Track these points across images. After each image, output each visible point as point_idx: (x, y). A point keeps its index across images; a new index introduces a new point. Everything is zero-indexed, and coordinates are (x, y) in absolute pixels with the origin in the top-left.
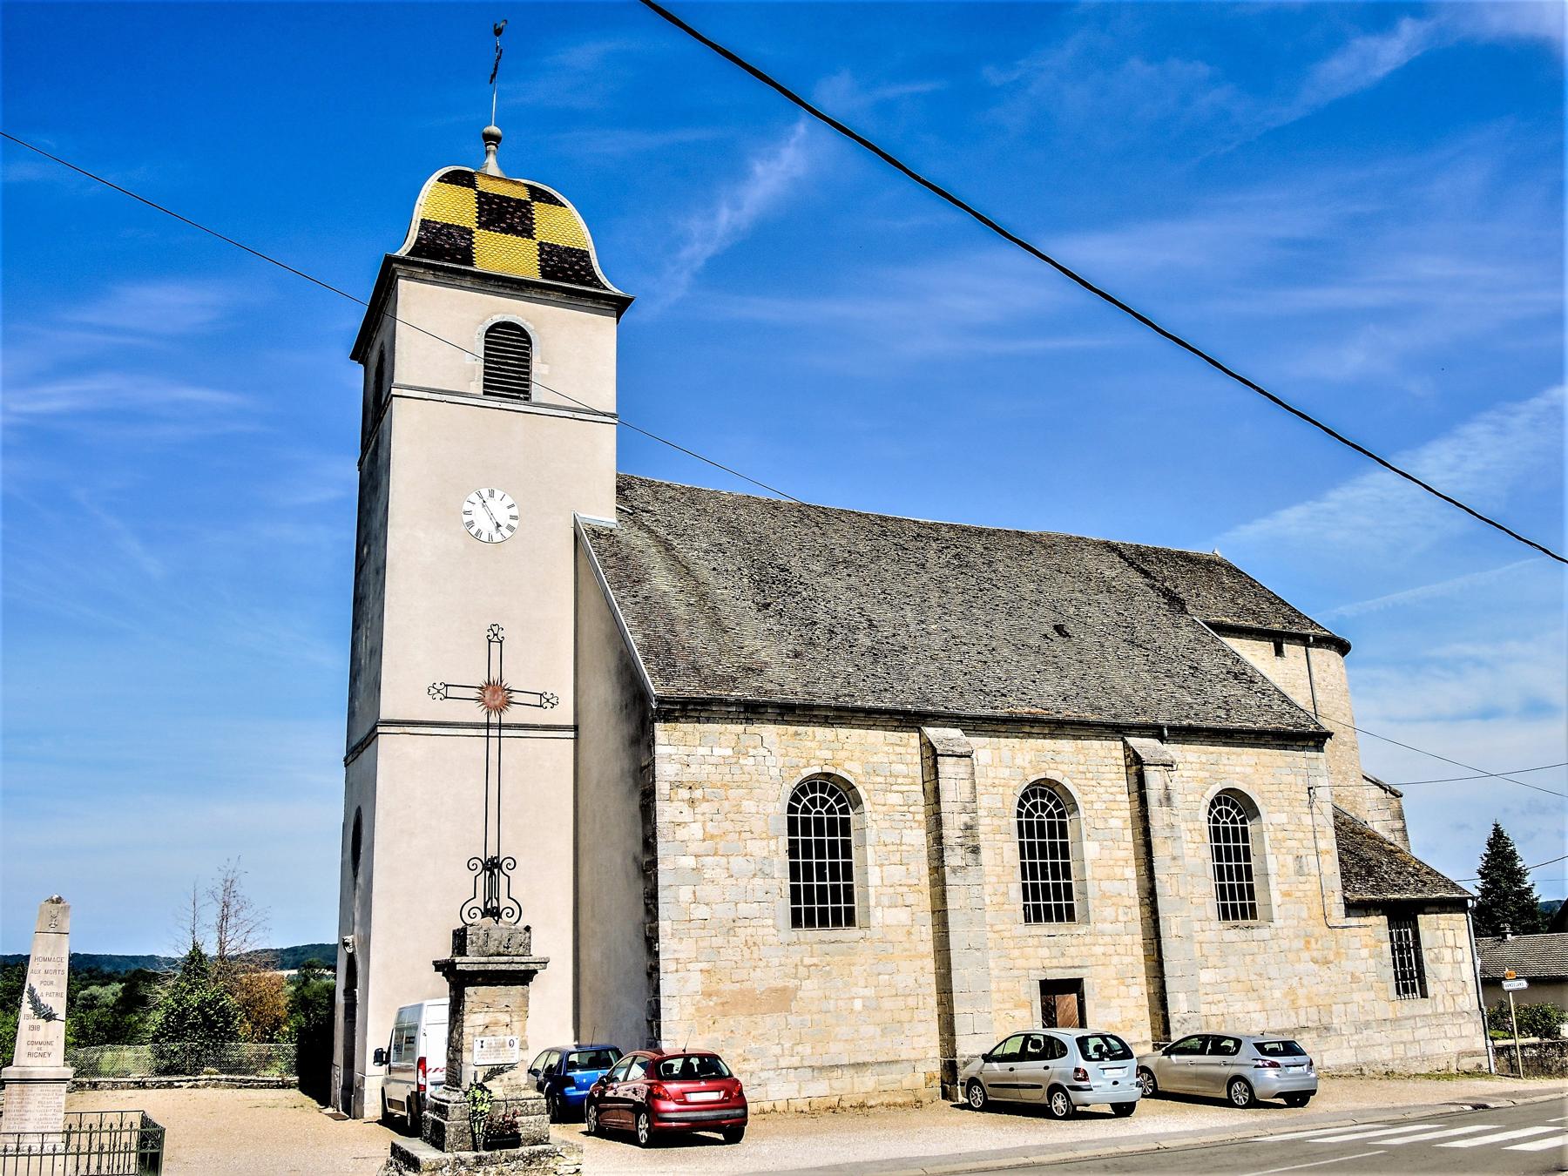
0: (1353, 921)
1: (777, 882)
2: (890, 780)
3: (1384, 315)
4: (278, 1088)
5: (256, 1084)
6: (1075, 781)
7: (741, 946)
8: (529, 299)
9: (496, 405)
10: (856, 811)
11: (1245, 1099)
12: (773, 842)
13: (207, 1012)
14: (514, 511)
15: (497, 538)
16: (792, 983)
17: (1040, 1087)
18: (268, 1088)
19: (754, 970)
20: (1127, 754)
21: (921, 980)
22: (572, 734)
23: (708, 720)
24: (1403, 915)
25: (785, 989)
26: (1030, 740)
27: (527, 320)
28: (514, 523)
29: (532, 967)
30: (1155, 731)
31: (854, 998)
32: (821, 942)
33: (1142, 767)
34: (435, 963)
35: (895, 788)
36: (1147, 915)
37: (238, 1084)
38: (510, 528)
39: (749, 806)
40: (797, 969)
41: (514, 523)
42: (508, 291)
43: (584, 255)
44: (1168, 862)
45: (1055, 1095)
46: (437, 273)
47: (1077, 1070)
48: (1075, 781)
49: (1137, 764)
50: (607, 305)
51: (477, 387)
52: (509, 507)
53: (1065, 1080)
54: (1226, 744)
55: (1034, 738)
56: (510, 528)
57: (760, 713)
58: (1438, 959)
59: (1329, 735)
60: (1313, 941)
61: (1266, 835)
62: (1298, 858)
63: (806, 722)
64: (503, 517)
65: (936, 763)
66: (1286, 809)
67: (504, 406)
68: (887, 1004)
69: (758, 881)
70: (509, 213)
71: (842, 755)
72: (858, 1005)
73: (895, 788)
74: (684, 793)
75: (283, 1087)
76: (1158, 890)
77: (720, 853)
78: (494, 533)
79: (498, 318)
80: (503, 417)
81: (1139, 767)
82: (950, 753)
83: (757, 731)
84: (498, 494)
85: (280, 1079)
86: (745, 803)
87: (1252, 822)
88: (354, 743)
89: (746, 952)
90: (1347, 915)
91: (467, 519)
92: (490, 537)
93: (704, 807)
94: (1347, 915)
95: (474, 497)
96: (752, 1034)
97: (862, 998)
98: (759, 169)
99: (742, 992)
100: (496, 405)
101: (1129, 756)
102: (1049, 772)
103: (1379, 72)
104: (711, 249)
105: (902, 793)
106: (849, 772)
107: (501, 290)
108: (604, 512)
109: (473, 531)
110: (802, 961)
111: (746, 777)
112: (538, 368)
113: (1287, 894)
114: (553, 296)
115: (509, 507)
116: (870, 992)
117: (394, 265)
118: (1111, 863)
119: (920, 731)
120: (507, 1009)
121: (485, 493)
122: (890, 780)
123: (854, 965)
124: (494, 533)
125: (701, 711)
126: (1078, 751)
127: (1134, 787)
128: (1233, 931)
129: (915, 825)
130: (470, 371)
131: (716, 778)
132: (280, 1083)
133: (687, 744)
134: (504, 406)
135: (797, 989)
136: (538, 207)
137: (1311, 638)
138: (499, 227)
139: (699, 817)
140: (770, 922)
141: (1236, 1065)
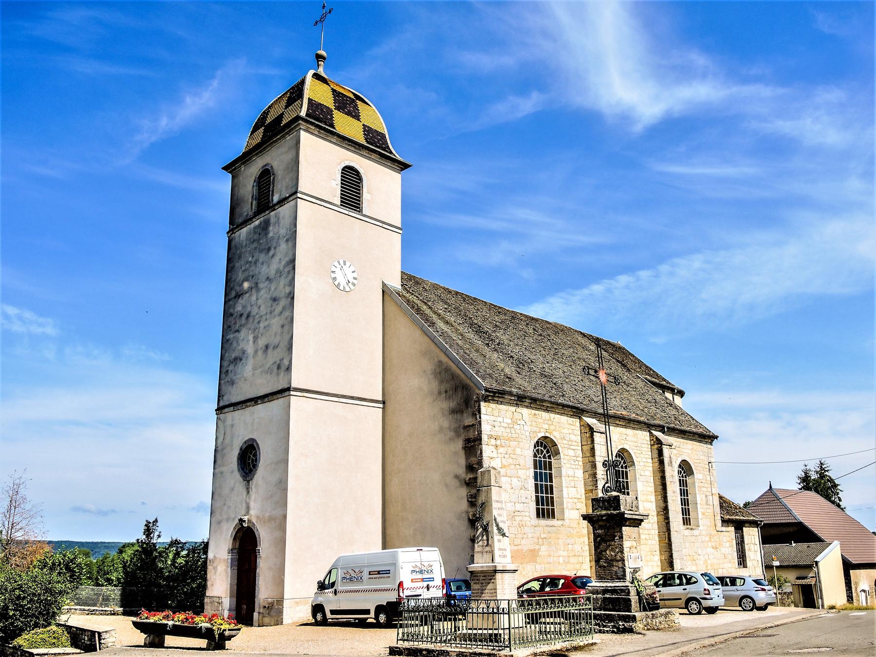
0: (724, 529)
1: (529, 493)
2: (570, 443)
3: (508, 236)
4: (111, 615)
5: (98, 612)
6: (634, 451)
7: (517, 526)
8: (362, 155)
9: (347, 212)
10: (555, 458)
11: (750, 607)
12: (528, 471)
13: (71, 565)
14: (355, 275)
15: (347, 289)
16: (537, 547)
17: (681, 599)
18: (105, 615)
19: (522, 539)
20: (651, 439)
21: (584, 548)
22: (381, 406)
23: (501, 403)
24: (739, 526)
25: (534, 550)
26: (618, 428)
27: (361, 167)
28: (355, 282)
29: (642, 518)
30: (662, 429)
31: (560, 556)
32: (547, 526)
33: (661, 446)
34: (582, 516)
35: (572, 447)
36: (662, 520)
37: (87, 612)
38: (354, 285)
39: (518, 451)
40: (538, 540)
41: (355, 282)
42: (352, 149)
43: (383, 136)
44: (672, 494)
45: (691, 603)
46: (321, 131)
47: (705, 590)
48: (634, 451)
49: (657, 444)
50: (397, 166)
51: (338, 201)
52: (353, 272)
53: (698, 594)
54: (682, 438)
55: (619, 427)
56: (354, 285)
57: (522, 401)
58: (749, 550)
59: (716, 437)
60: (712, 537)
61: (696, 484)
62: (706, 496)
63: (539, 408)
64: (350, 277)
65: (592, 436)
66: (702, 472)
67: (351, 214)
68: (572, 560)
69: (523, 492)
70: (348, 104)
71: (552, 427)
72: (561, 561)
73: (572, 447)
74: (493, 442)
75: (114, 614)
76: (670, 508)
77: (508, 475)
78: (346, 286)
79: (347, 163)
80: (346, 220)
81: (660, 445)
82: (598, 431)
83: (520, 411)
84: (348, 264)
85: (112, 609)
86: (517, 449)
87: (689, 477)
88: (221, 404)
89: (519, 529)
90: (722, 526)
91: (333, 275)
92: (344, 288)
93: (501, 450)
94: (722, 526)
95: (336, 264)
96: (523, 574)
97: (563, 556)
98: (188, 100)
99: (518, 551)
100: (347, 212)
101: (653, 440)
102: (625, 445)
103: (520, 115)
104: (154, 139)
105: (574, 450)
106: (555, 437)
107: (350, 148)
108: (395, 283)
109: (336, 283)
110: (540, 536)
111: (517, 436)
112: (366, 196)
113: (703, 514)
114: (374, 156)
115: (353, 272)
116: (565, 553)
117: (300, 122)
118: (646, 493)
119: (580, 418)
120: (635, 539)
121: (342, 263)
122: (570, 443)
123: (558, 539)
124: (346, 286)
125: (500, 397)
126: (634, 435)
127: (656, 456)
128: (687, 530)
129: (579, 467)
130: (333, 190)
131: (505, 434)
132: (112, 612)
133: (494, 415)
134: (351, 214)
135: (539, 550)
136: (359, 103)
137: (676, 390)
138: (344, 110)
139: (499, 455)
140: (527, 514)
141: (744, 590)
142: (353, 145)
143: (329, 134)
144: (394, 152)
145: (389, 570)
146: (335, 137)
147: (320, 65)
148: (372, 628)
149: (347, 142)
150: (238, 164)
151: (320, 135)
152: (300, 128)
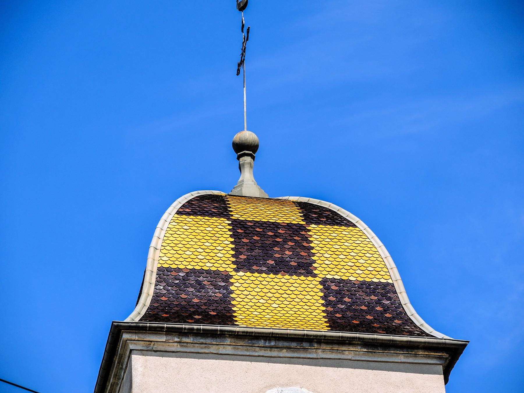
42: (284, 353)
46: (185, 340)
50: (428, 357)
107: (275, 353)
114: (349, 353)
117: (125, 336)
142: (280, 344)
143: (208, 341)
144: (427, 328)
145: (468, 342)
146: (228, 341)
147: (243, 164)
148: (444, 378)
149: (262, 343)
150: (437, 354)
151: (188, 350)
152: (131, 351)
